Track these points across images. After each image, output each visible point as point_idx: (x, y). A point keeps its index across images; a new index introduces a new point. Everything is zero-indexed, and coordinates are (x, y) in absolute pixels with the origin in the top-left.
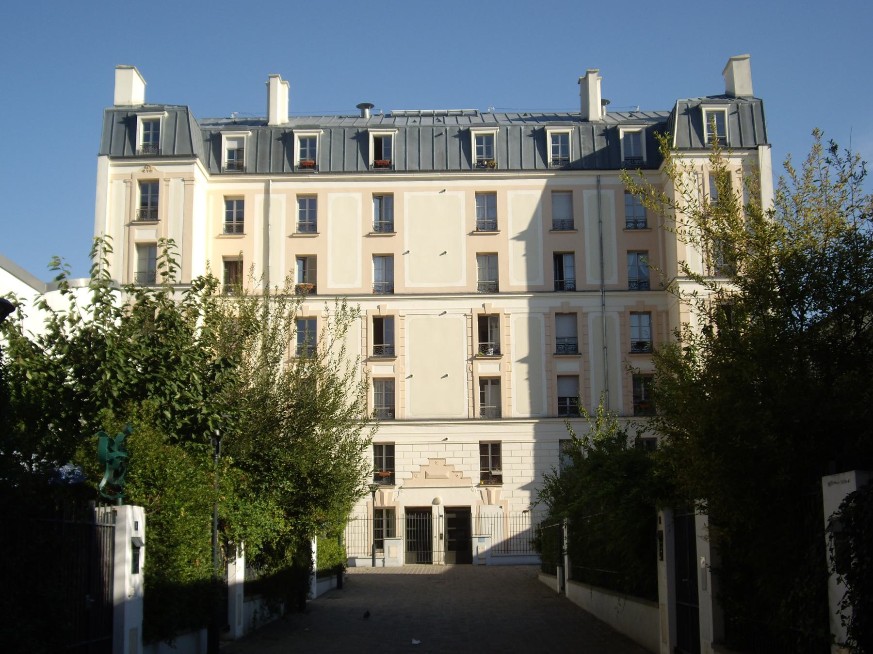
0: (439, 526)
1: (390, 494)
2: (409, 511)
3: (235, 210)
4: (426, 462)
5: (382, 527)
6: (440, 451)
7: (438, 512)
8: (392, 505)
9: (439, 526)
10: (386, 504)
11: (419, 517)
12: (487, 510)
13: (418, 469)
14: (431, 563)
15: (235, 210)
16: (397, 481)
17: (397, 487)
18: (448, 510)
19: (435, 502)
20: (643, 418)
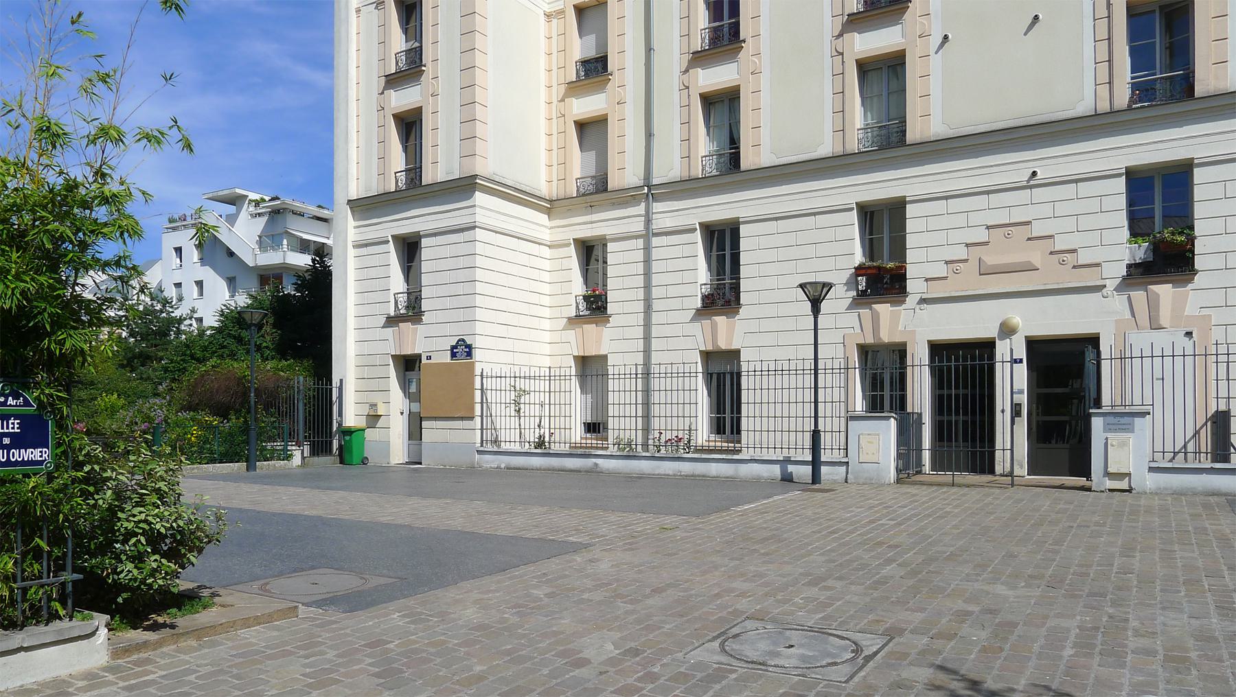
0: (1012, 382)
1: (895, 319)
2: (938, 349)
3: (728, 416)
4: (982, 235)
5: (882, 389)
6: (1015, 207)
7: (1010, 351)
8: (898, 339)
9: (1012, 382)
10: (886, 337)
11: (962, 367)
12: (1141, 340)
13: (962, 253)
14: (992, 471)
15: (728, 416)
16: (911, 286)
17: (911, 301)
18: (1033, 344)
19: (1007, 330)
20: (182, 588)
